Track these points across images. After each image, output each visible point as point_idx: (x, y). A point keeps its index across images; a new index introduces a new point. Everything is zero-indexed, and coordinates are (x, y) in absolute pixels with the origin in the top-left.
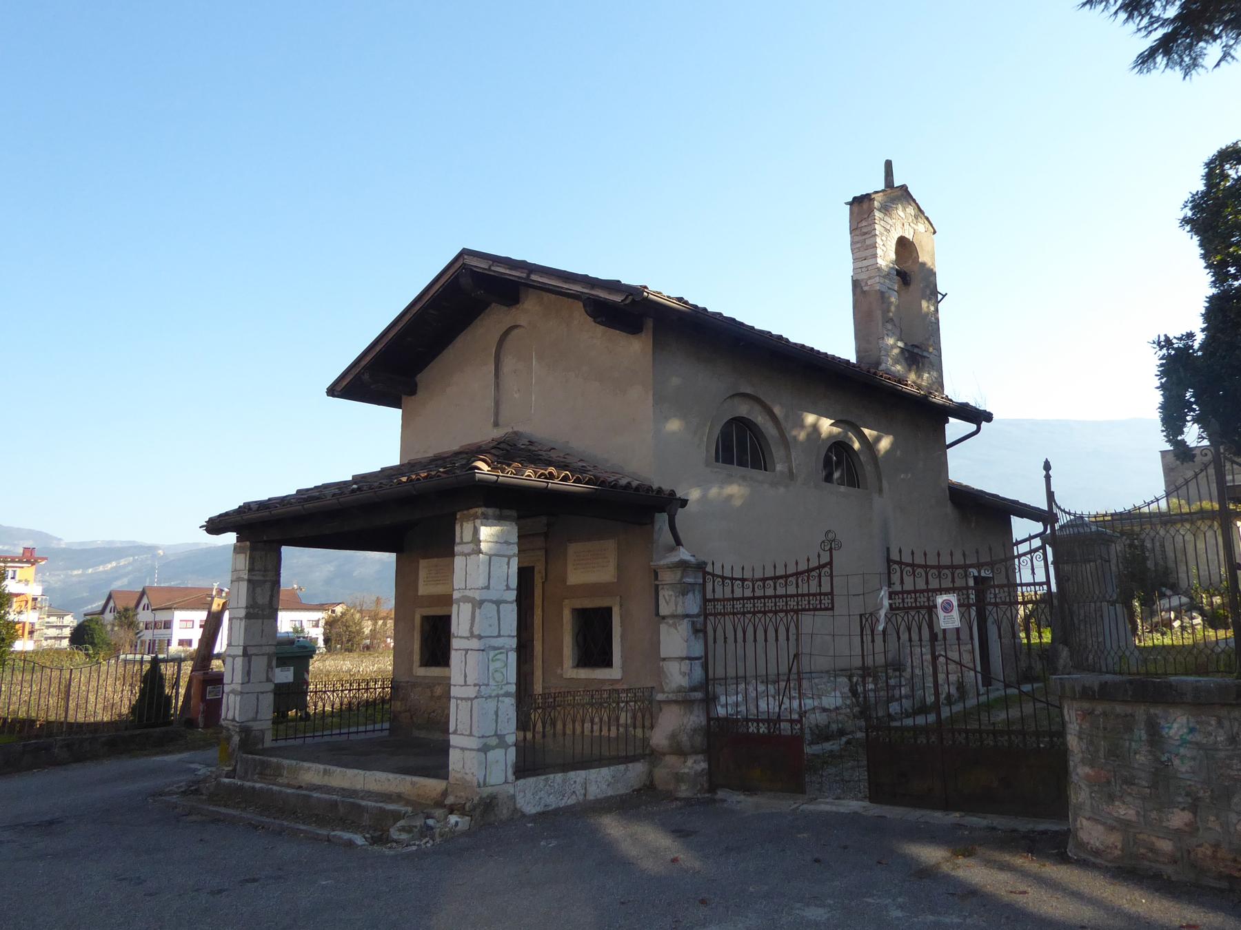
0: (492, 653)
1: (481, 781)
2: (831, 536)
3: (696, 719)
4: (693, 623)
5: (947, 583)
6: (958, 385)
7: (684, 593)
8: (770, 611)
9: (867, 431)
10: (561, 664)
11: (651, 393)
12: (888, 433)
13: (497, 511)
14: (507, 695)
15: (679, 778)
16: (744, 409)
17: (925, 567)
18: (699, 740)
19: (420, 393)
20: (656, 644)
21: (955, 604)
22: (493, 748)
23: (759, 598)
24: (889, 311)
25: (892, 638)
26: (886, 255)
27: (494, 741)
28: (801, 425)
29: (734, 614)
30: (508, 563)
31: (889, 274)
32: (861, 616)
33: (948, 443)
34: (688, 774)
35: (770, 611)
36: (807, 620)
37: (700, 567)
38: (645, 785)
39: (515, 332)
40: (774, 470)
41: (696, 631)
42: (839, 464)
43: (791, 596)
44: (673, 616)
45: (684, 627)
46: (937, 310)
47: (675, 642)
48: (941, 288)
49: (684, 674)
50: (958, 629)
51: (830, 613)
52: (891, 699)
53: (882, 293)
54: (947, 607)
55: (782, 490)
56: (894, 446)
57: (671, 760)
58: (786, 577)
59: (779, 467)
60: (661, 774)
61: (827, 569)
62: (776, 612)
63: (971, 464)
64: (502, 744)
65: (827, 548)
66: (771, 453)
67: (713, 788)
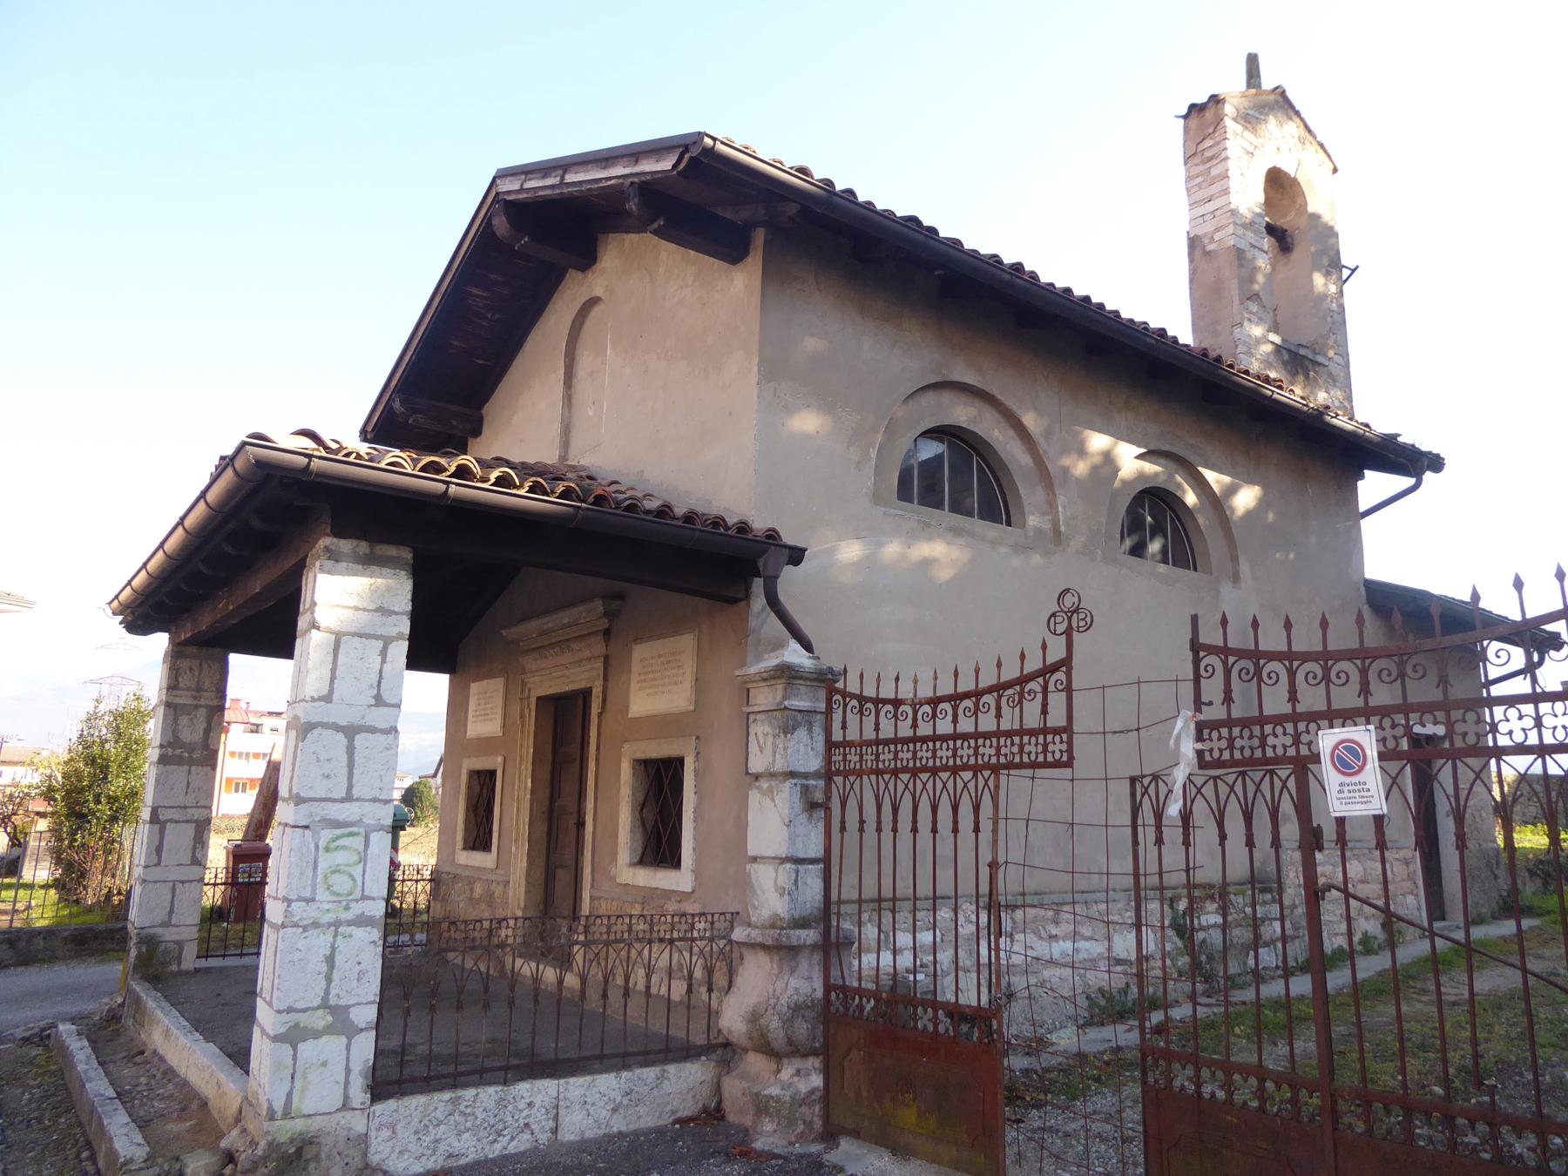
0: (326, 835)
1: (279, 1106)
2: (1069, 600)
3: (805, 982)
4: (806, 790)
5: (1347, 697)
6: (1375, 403)
7: (787, 729)
8: (945, 768)
9: (1211, 476)
10: (614, 857)
11: (756, 361)
12: (1251, 481)
13: (363, 547)
14: (362, 921)
15: (762, 1107)
16: (962, 413)
17: (1288, 656)
18: (802, 1029)
19: (485, 431)
20: (741, 827)
21: (1372, 752)
22: (317, 1034)
23: (924, 740)
24: (1252, 280)
25: (1205, 832)
26: (1248, 195)
27: (321, 1020)
28: (1082, 452)
29: (879, 772)
30: (383, 653)
31: (1252, 223)
32: (1133, 780)
33: (1362, 508)
34: (777, 1099)
35: (945, 768)
36: (1015, 785)
37: (826, 680)
38: (705, 1110)
39: (596, 311)
40: (1023, 525)
41: (812, 806)
42: (1158, 529)
43: (1000, 733)
44: (771, 775)
45: (787, 794)
46: (1341, 293)
47: (773, 824)
48: (1346, 260)
49: (781, 891)
50: (1379, 820)
51: (1066, 772)
52: (1256, 943)
53: (1239, 253)
54: (1349, 761)
55: (1036, 559)
56: (1263, 504)
57: (756, 1063)
58: (977, 694)
59: (1033, 521)
60: (733, 1088)
61: (1060, 675)
62: (955, 771)
63: (1405, 542)
64: (341, 1023)
65: (1062, 628)
66: (1019, 496)
67: (830, 1136)
